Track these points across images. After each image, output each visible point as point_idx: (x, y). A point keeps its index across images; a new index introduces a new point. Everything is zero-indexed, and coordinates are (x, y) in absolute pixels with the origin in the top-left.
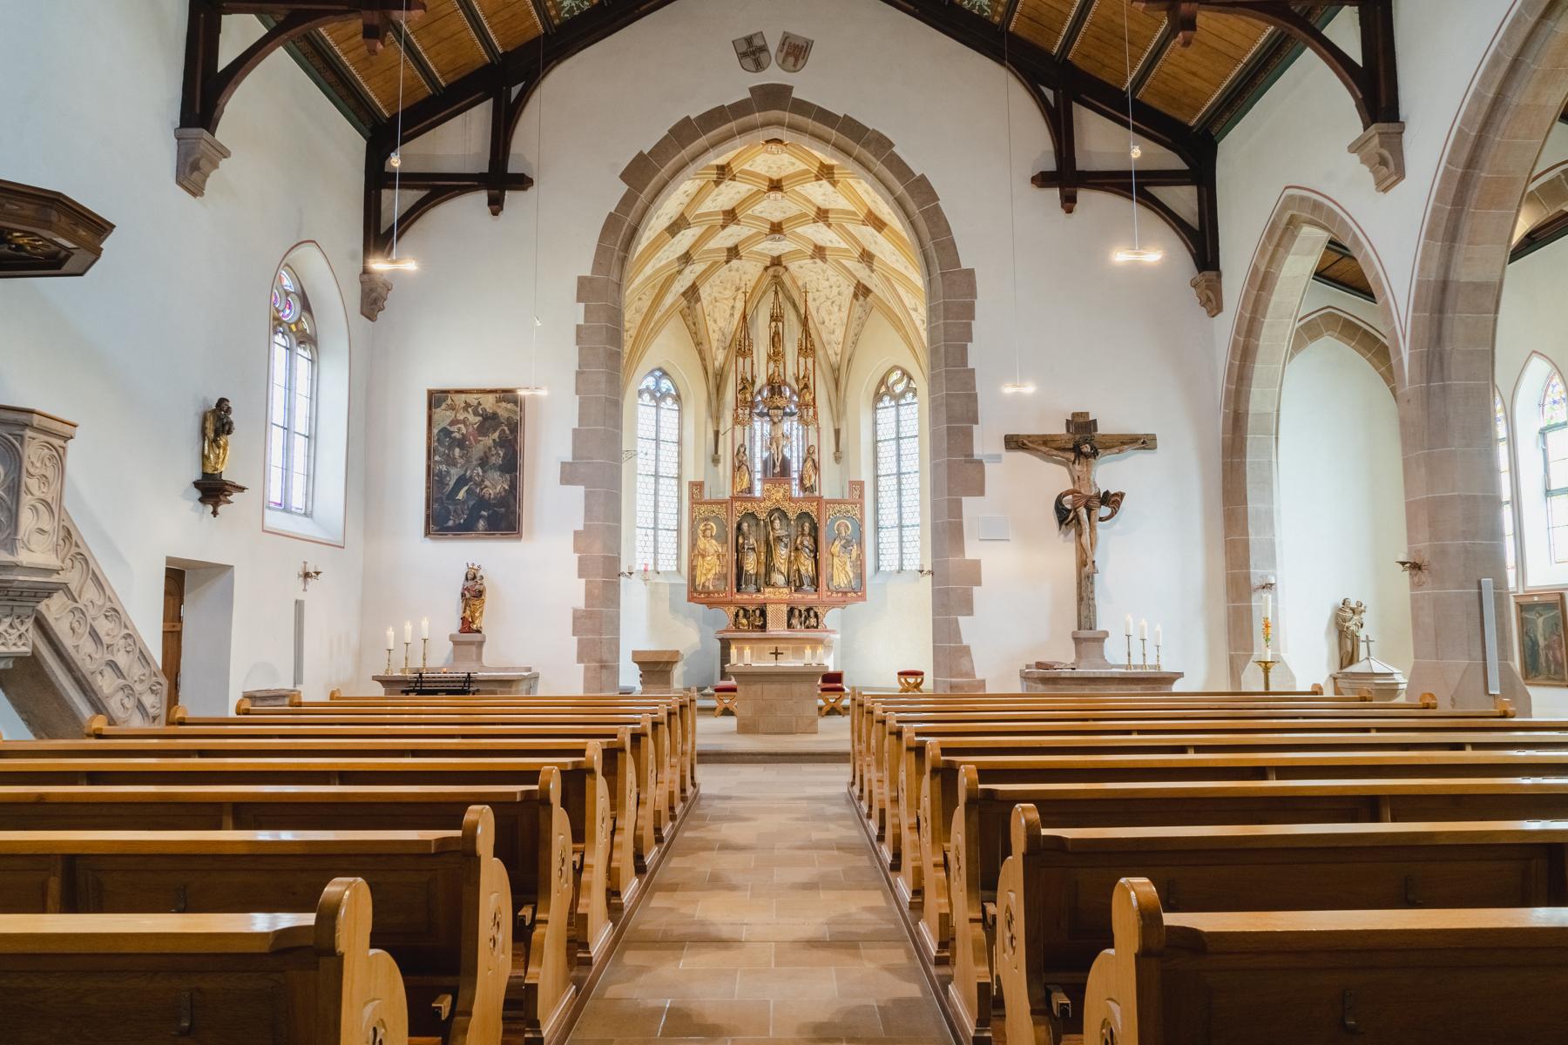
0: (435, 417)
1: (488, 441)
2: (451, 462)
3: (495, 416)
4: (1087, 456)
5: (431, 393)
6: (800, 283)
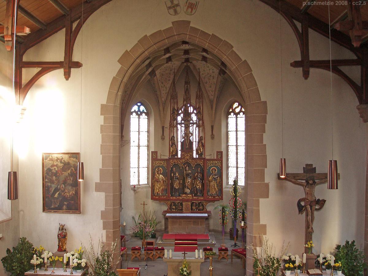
4: (311, 184)
6: (197, 68)
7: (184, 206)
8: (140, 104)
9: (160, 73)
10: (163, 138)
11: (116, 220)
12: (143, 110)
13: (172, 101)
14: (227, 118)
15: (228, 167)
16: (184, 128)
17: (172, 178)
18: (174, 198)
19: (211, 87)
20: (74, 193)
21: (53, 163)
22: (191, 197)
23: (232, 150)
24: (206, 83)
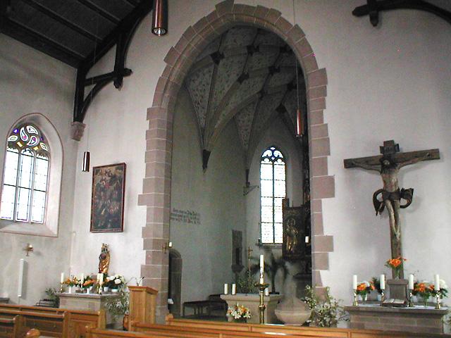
1: (112, 188)
2: (100, 198)
4: (388, 167)
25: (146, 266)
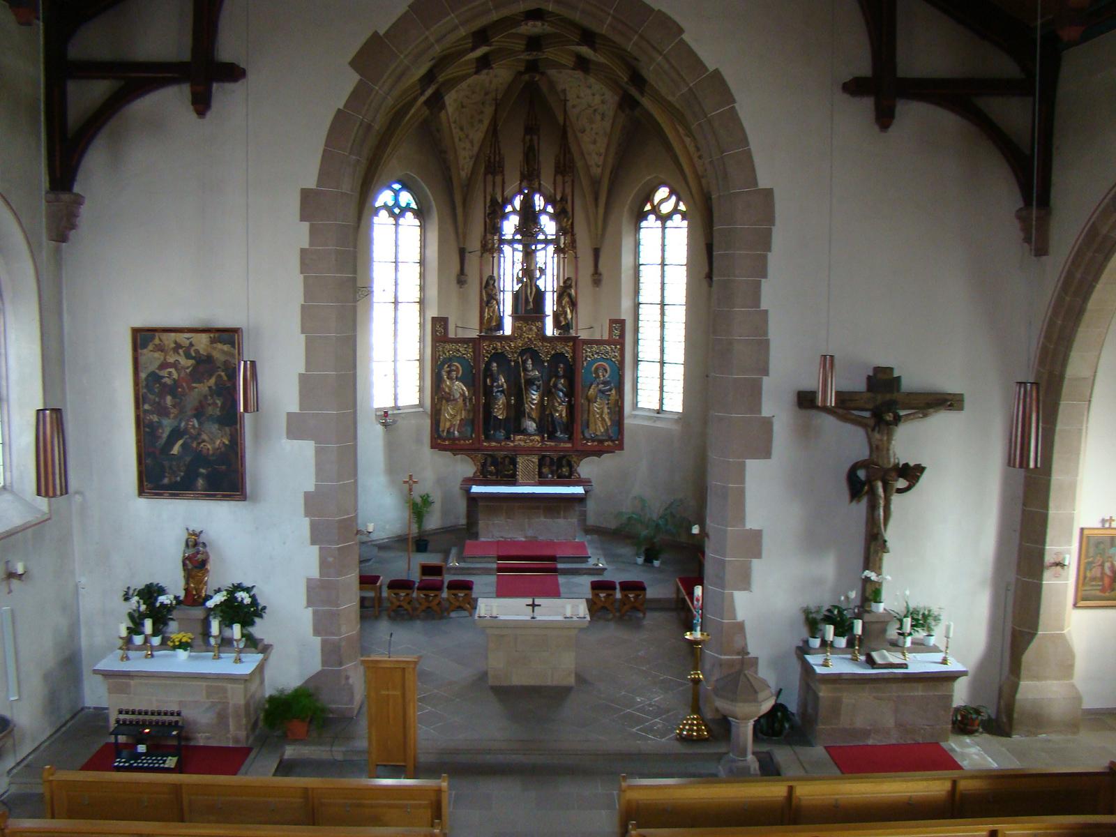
0: (142, 360)
1: (202, 388)
2: (163, 412)
3: (209, 359)
5: (136, 332)
6: (560, 88)
7: (520, 466)
8: (400, 187)
9: (455, 100)
10: (461, 280)
11: (346, 517)
12: (408, 204)
13: (490, 177)
14: (637, 229)
15: (636, 362)
16: (521, 254)
17: (488, 392)
18: (494, 444)
19: (595, 142)
20: (227, 443)
21: (165, 359)
22: (539, 442)
23: (649, 316)
24: (583, 131)
25: (319, 580)
